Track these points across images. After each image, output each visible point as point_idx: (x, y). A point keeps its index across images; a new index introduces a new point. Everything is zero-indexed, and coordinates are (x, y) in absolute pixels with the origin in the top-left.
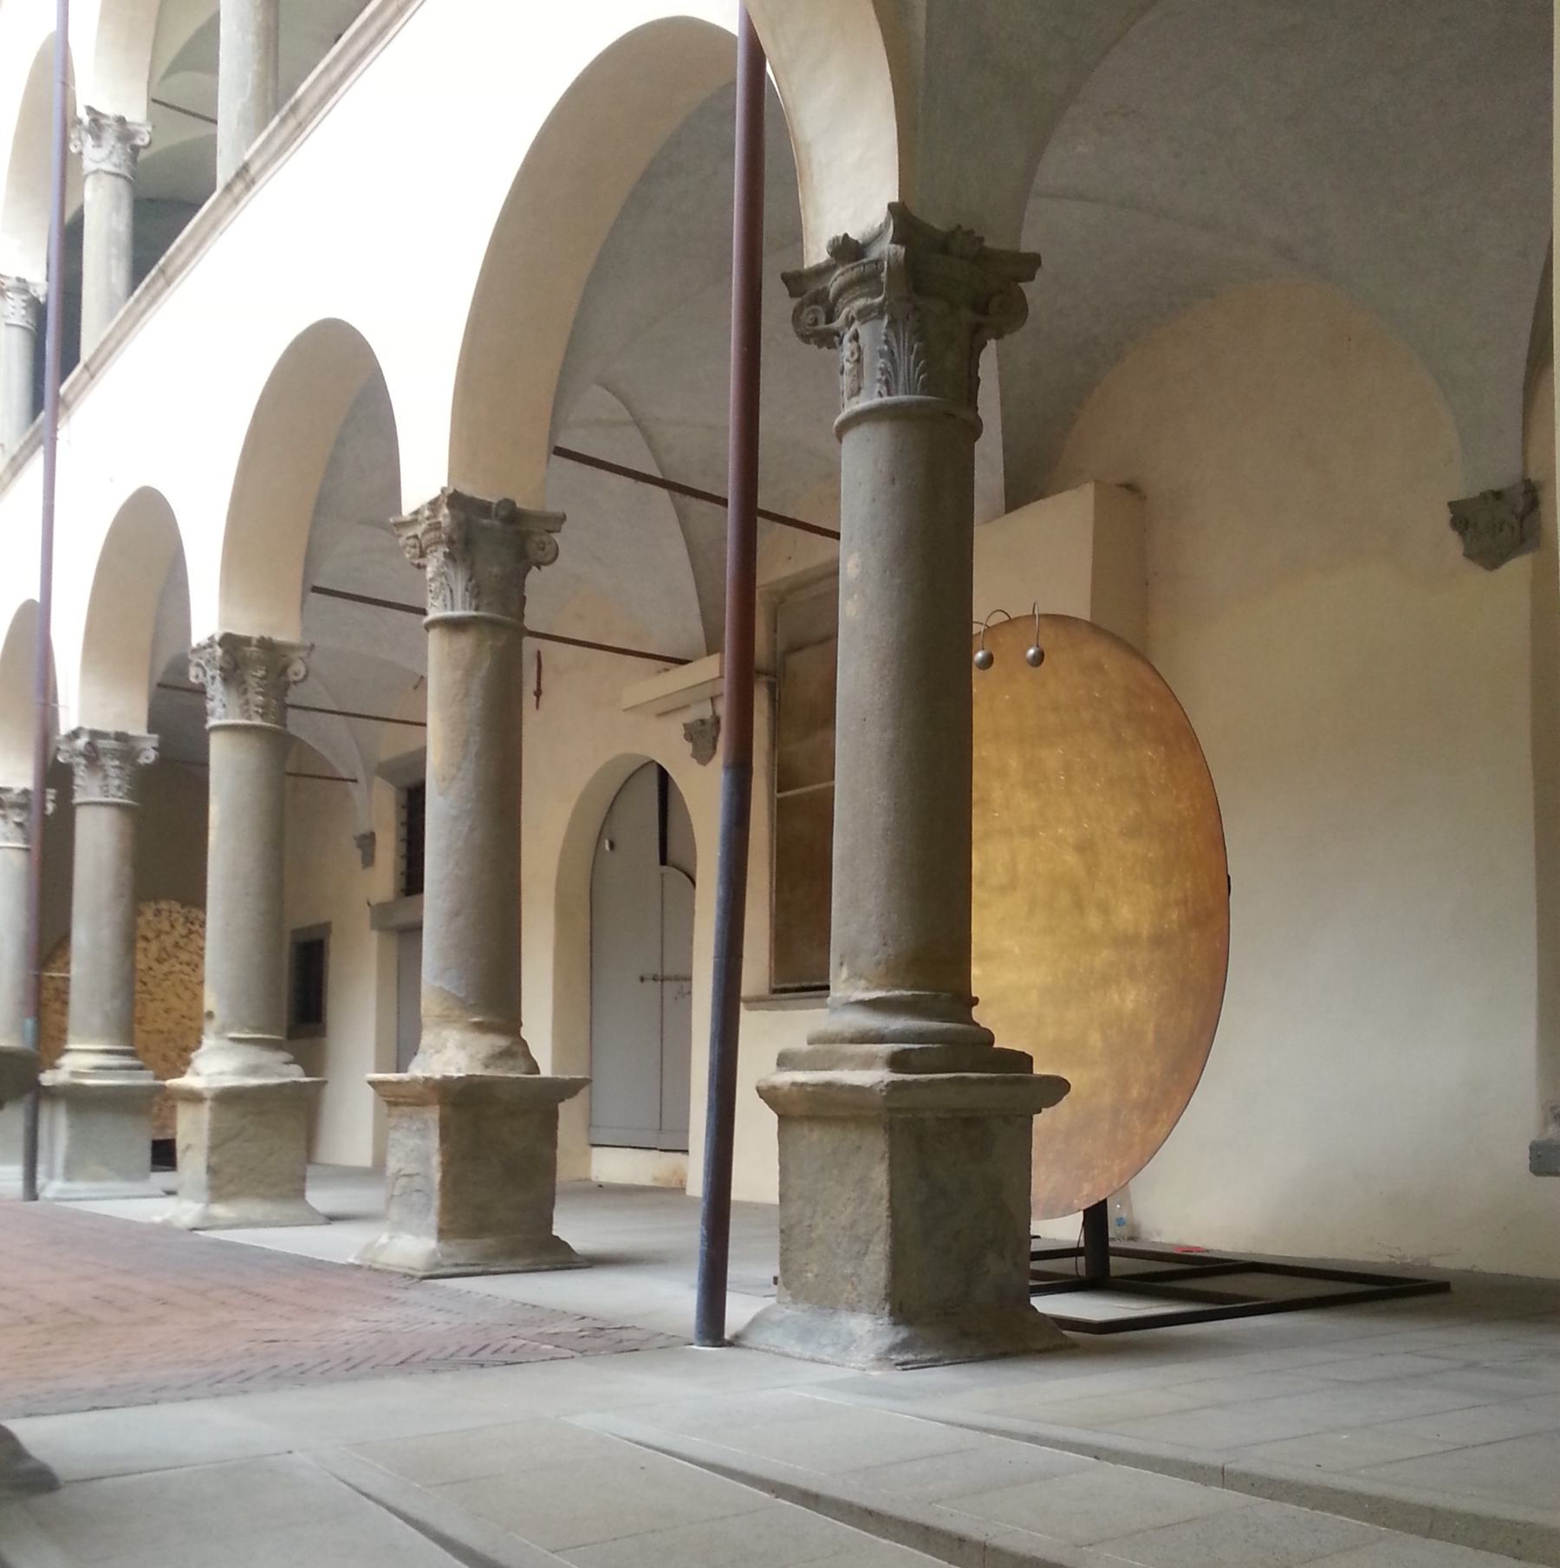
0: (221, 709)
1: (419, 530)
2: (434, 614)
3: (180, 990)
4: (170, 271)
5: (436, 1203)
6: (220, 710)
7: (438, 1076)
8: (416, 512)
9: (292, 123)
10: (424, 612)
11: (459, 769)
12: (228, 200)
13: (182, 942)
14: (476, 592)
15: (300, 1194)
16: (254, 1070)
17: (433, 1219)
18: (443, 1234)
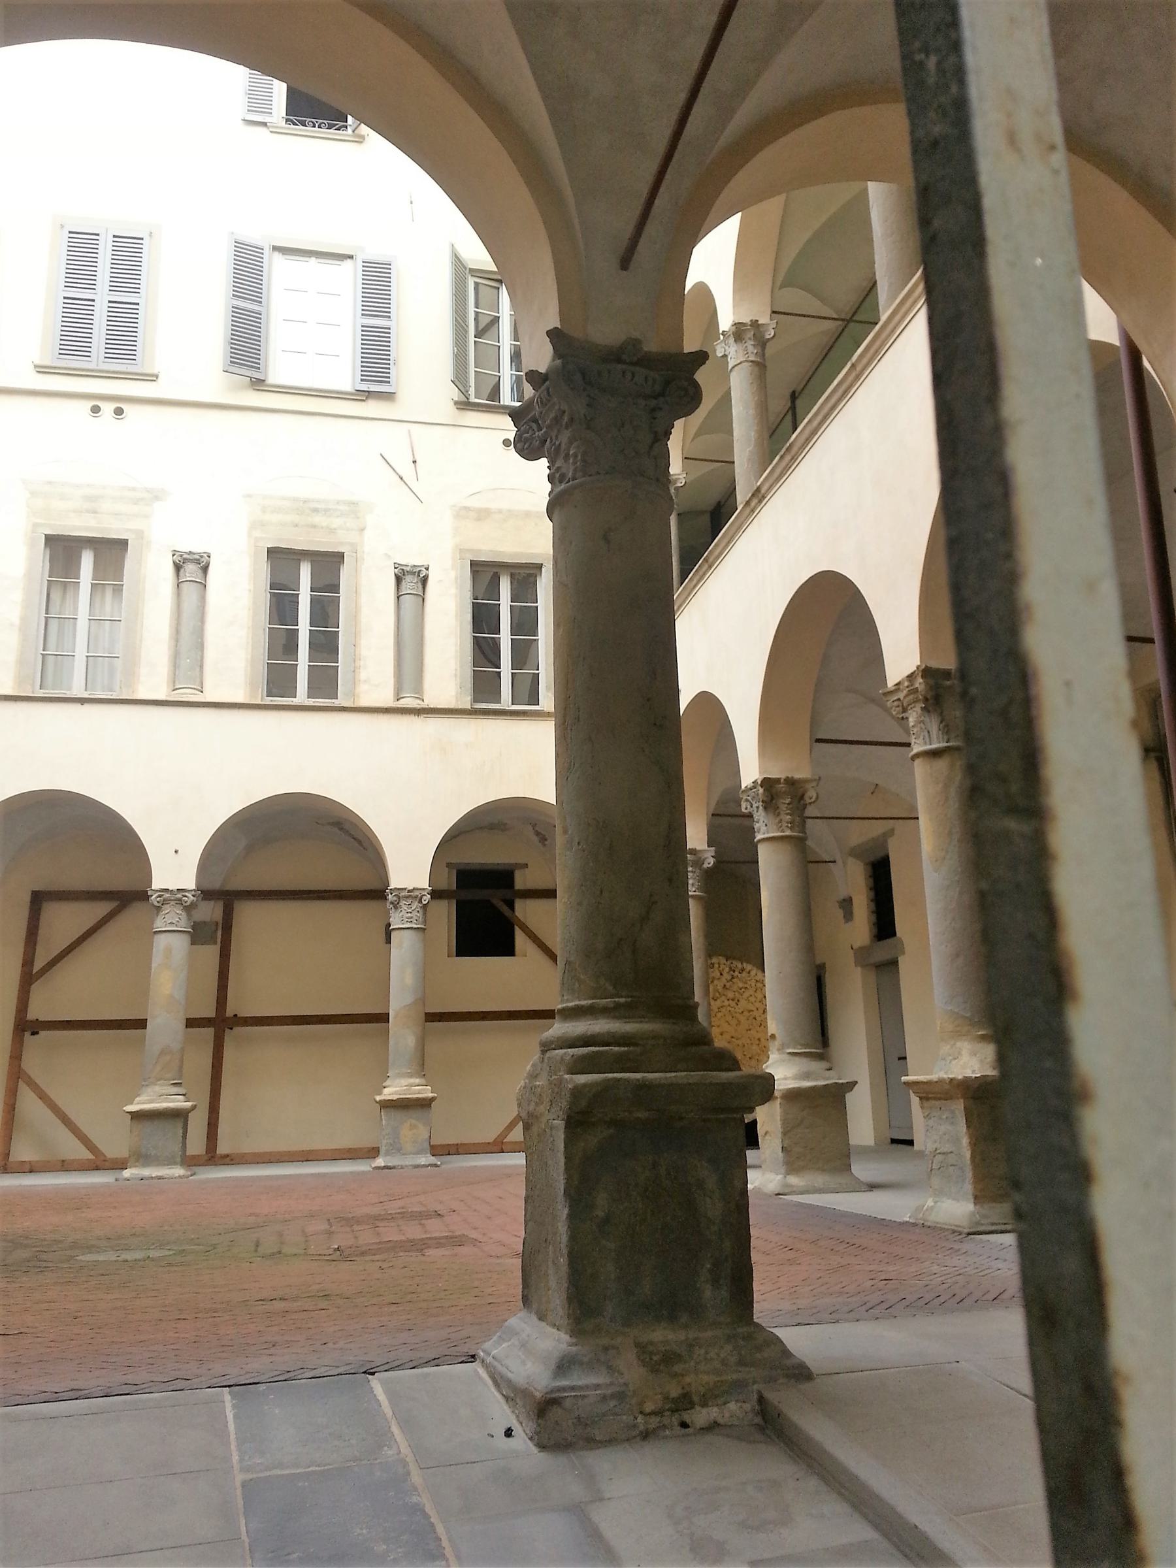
0: (764, 827)
1: (901, 695)
2: (916, 749)
3: (729, 1018)
4: (711, 560)
5: (969, 1174)
6: (764, 828)
7: (960, 1077)
8: (898, 684)
9: (788, 458)
10: (909, 745)
11: (947, 852)
12: (748, 510)
13: (728, 985)
14: (946, 729)
15: (848, 1167)
16: (807, 1076)
17: (968, 1187)
18: (977, 1199)
